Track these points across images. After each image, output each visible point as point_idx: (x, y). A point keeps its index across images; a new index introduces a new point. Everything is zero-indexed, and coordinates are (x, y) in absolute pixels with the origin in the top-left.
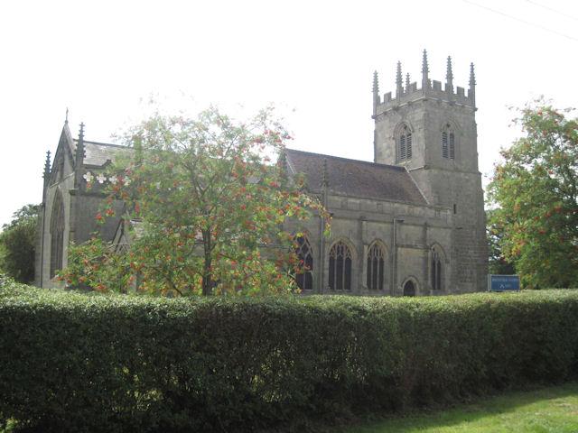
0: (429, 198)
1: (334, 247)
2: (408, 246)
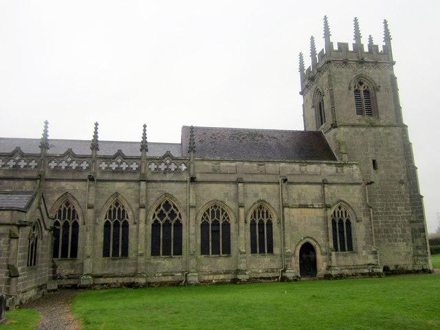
1: (208, 211)
2: (301, 206)
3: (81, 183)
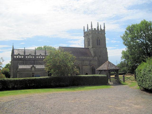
0: (93, 55)
2: (86, 66)
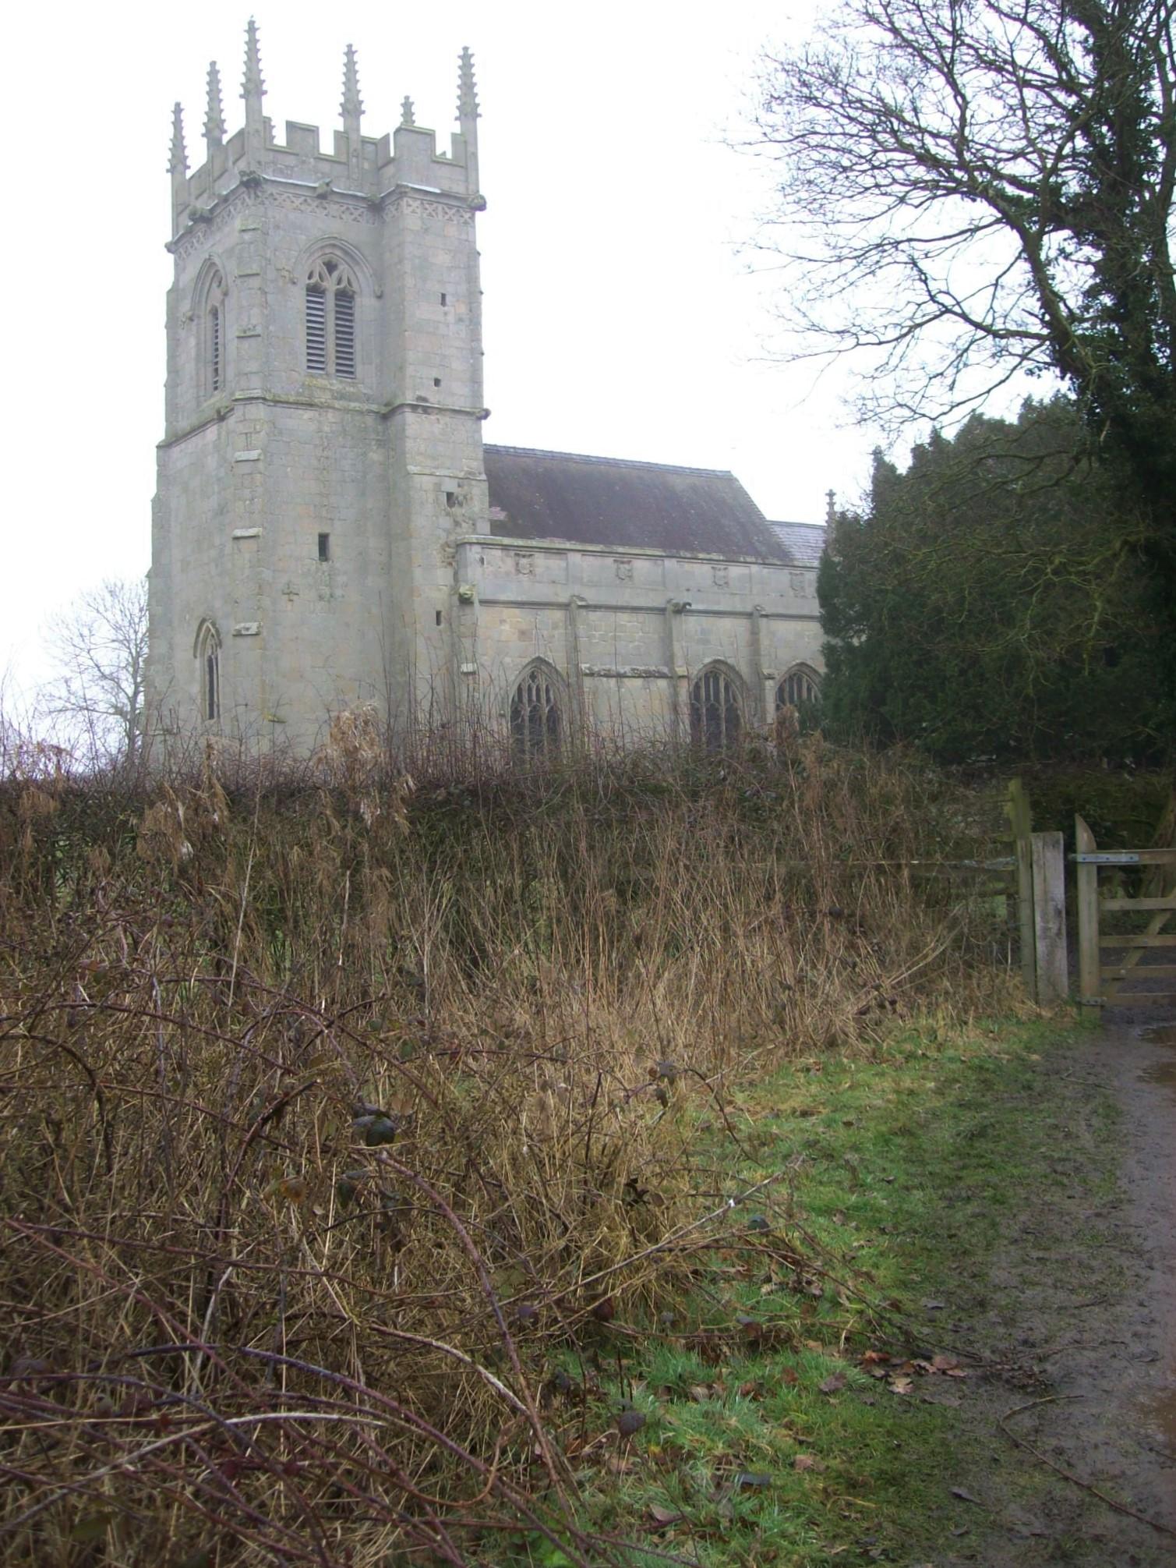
3: (634, 617)
